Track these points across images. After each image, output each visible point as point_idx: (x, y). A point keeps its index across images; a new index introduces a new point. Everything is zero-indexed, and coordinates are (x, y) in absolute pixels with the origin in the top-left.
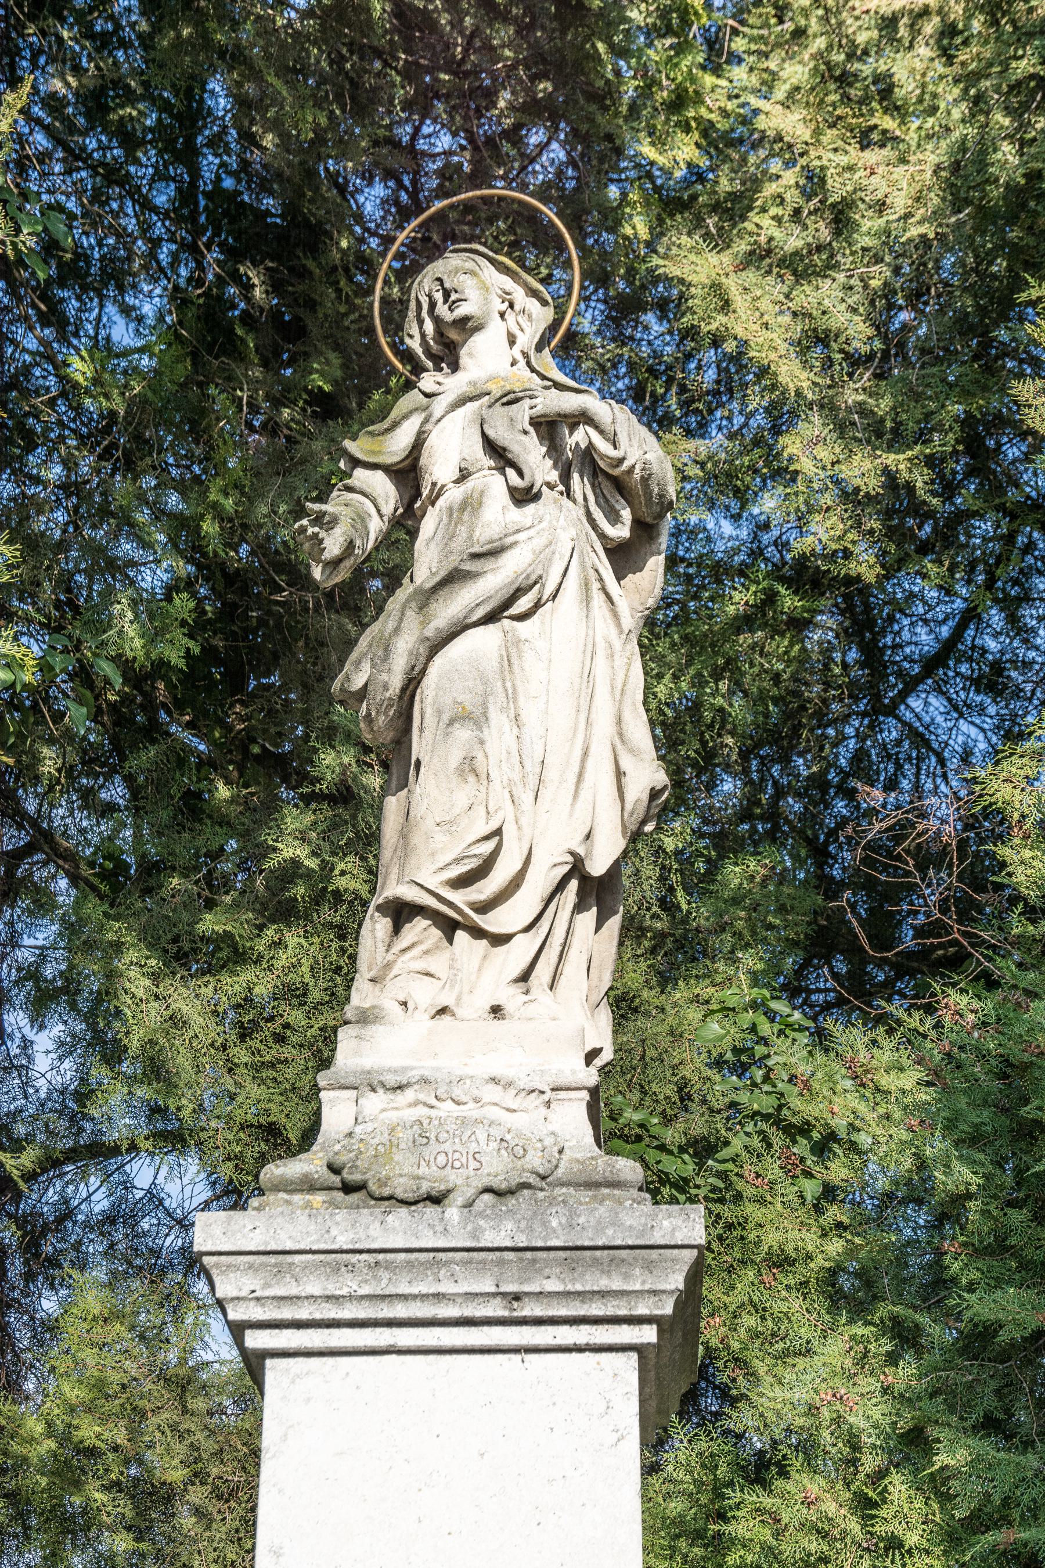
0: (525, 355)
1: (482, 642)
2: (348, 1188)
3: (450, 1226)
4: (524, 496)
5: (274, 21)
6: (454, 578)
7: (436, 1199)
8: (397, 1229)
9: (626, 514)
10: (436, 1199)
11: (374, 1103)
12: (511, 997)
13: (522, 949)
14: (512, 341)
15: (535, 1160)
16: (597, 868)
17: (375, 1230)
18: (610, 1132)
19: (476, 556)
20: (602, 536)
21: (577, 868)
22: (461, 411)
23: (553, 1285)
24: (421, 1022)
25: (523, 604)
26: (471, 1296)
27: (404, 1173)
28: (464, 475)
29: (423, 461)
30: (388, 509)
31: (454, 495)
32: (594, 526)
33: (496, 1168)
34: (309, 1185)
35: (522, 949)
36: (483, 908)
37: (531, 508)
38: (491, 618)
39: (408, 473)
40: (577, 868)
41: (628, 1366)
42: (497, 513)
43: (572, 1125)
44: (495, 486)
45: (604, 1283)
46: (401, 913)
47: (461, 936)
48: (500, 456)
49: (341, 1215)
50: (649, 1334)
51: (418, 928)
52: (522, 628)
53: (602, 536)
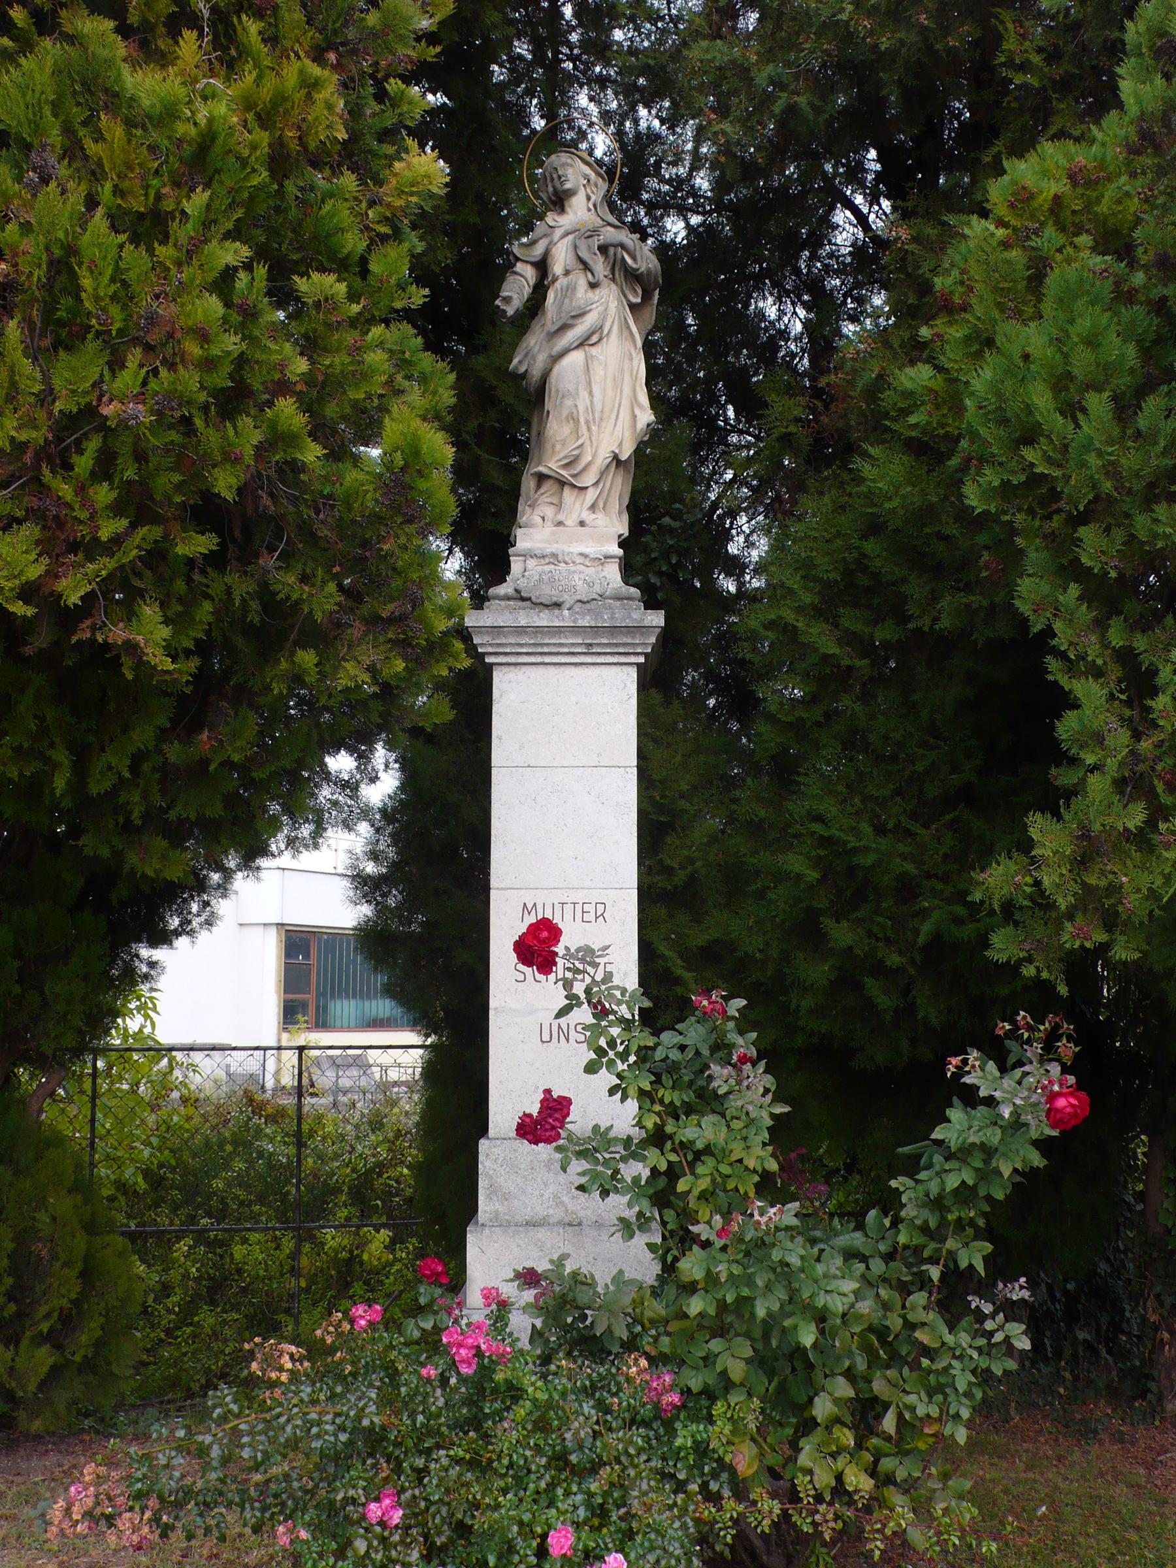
0: (595, 206)
1: (576, 357)
2: (523, 599)
3: (564, 619)
4: (593, 286)
5: (130, 482)
6: (564, 327)
7: (558, 605)
8: (543, 619)
9: (640, 291)
10: (558, 605)
11: (531, 563)
12: (586, 516)
13: (591, 495)
14: (589, 198)
15: (597, 588)
16: (624, 457)
17: (535, 618)
18: (628, 570)
19: (573, 317)
20: (628, 301)
21: (616, 457)
22: (566, 240)
23: (605, 641)
24: (549, 529)
25: (595, 339)
26: (573, 645)
27: (547, 593)
28: (567, 273)
29: (549, 261)
30: (532, 283)
31: (562, 282)
32: (625, 296)
33: (583, 593)
34: (507, 598)
35: (591, 495)
36: (574, 476)
37: (597, 291)
38: (581, 345)
39: (542, 266)
40: (616, 457)
41: (633, 673)
42: (582, 292)
43: (613, 573)
44: (581, 280)
45: (625, 640)
46: (541, 478)
47: (567, 490)
48: (586, 267)
49: (522, 612)
50: (642, 660)
51: (547, 486)
52: (594, 351)
53: (628, 301)
